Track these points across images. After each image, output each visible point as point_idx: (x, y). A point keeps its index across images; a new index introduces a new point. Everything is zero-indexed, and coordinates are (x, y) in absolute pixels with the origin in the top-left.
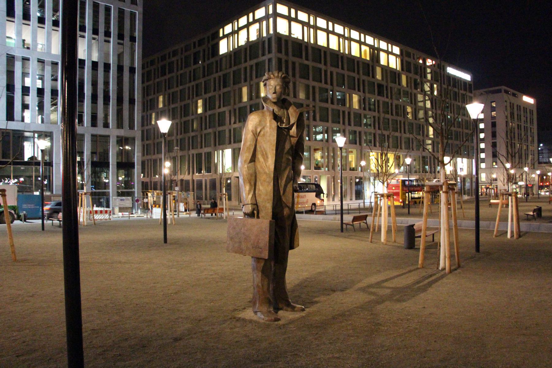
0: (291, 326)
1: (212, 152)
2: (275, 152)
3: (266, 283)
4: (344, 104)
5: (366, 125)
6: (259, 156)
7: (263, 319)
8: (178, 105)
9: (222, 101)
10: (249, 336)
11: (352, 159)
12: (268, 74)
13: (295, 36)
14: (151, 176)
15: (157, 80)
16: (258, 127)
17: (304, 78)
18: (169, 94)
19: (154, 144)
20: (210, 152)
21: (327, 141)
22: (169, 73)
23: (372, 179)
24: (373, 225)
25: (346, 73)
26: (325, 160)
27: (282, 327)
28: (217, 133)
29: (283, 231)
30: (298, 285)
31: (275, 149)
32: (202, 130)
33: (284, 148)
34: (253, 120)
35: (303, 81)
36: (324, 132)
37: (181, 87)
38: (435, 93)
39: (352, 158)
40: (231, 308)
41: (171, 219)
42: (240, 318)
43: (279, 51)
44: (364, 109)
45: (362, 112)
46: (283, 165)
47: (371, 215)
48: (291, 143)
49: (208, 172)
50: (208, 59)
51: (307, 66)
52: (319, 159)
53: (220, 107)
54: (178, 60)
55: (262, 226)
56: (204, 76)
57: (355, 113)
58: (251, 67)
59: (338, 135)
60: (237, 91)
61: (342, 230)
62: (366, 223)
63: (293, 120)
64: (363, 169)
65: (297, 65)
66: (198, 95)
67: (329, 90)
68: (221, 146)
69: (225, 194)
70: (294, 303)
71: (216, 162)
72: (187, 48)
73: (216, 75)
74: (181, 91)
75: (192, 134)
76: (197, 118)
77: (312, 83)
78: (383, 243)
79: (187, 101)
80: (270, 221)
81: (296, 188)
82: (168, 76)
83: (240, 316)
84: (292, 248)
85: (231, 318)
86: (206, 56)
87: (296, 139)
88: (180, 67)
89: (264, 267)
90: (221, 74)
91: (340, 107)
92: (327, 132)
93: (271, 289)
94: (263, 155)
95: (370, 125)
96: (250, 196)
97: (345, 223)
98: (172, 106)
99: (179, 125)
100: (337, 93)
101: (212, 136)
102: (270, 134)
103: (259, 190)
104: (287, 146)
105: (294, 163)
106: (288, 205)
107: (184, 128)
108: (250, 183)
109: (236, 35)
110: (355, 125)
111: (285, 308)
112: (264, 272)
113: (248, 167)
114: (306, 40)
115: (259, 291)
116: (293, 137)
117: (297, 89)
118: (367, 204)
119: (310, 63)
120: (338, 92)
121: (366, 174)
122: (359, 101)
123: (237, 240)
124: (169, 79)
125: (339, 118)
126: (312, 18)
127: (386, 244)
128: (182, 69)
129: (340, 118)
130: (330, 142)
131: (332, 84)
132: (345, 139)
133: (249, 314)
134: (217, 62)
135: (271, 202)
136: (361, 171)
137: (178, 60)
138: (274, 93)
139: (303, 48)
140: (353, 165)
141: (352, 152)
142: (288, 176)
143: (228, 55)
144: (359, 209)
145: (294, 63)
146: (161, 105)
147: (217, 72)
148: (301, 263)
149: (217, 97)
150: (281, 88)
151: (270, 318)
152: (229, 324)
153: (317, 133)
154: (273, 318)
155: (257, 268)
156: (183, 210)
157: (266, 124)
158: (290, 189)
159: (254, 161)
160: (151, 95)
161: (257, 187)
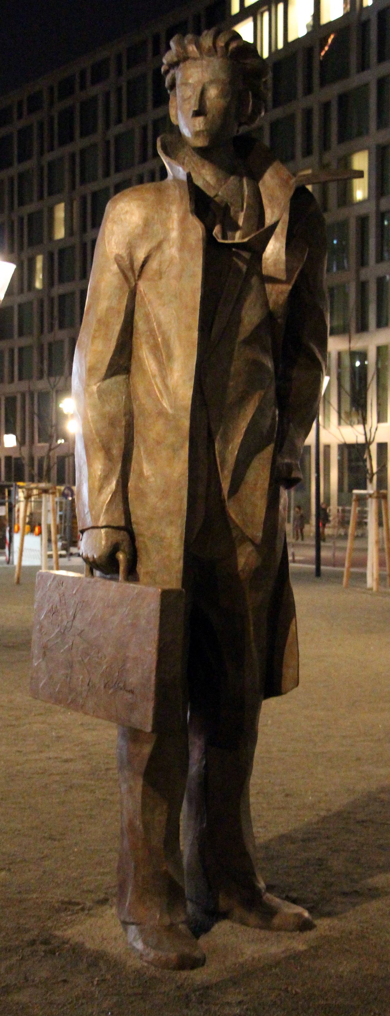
2: (196, 334)
6: (145, 355)
12: (180, 44)
14: (32, 442)
15: (48, 157)
19: (41, 347)
22: (83, 134)
30: (339, 814)
31: (195, 324)
33: (239, 322)
40: (57, 895)
46: (234, 386)
48: (266, 303)
54: (107, 95)
58: (326, 106)
82: (79, 143)
84: (273, 686)
85: (33, 943)
87: (288, 288)
88: (113, 116)
89: (152, 758)
94: (155, 349)
103: (141, 474)
104: (250, 316)
105: (282, 376)
106: (249, 532)
108: (107, 451)
109: (281, 6)
111: (238, 912)
113: (99, 391)
116: (273, 280)
124: (83, 152)
135: (181, 521)
137: (107, 95)
150: (223, 94)
154: (173, 955)
155: (130, 762)
157: (167, 232)
159: (127, 370)
160: (31, 200)
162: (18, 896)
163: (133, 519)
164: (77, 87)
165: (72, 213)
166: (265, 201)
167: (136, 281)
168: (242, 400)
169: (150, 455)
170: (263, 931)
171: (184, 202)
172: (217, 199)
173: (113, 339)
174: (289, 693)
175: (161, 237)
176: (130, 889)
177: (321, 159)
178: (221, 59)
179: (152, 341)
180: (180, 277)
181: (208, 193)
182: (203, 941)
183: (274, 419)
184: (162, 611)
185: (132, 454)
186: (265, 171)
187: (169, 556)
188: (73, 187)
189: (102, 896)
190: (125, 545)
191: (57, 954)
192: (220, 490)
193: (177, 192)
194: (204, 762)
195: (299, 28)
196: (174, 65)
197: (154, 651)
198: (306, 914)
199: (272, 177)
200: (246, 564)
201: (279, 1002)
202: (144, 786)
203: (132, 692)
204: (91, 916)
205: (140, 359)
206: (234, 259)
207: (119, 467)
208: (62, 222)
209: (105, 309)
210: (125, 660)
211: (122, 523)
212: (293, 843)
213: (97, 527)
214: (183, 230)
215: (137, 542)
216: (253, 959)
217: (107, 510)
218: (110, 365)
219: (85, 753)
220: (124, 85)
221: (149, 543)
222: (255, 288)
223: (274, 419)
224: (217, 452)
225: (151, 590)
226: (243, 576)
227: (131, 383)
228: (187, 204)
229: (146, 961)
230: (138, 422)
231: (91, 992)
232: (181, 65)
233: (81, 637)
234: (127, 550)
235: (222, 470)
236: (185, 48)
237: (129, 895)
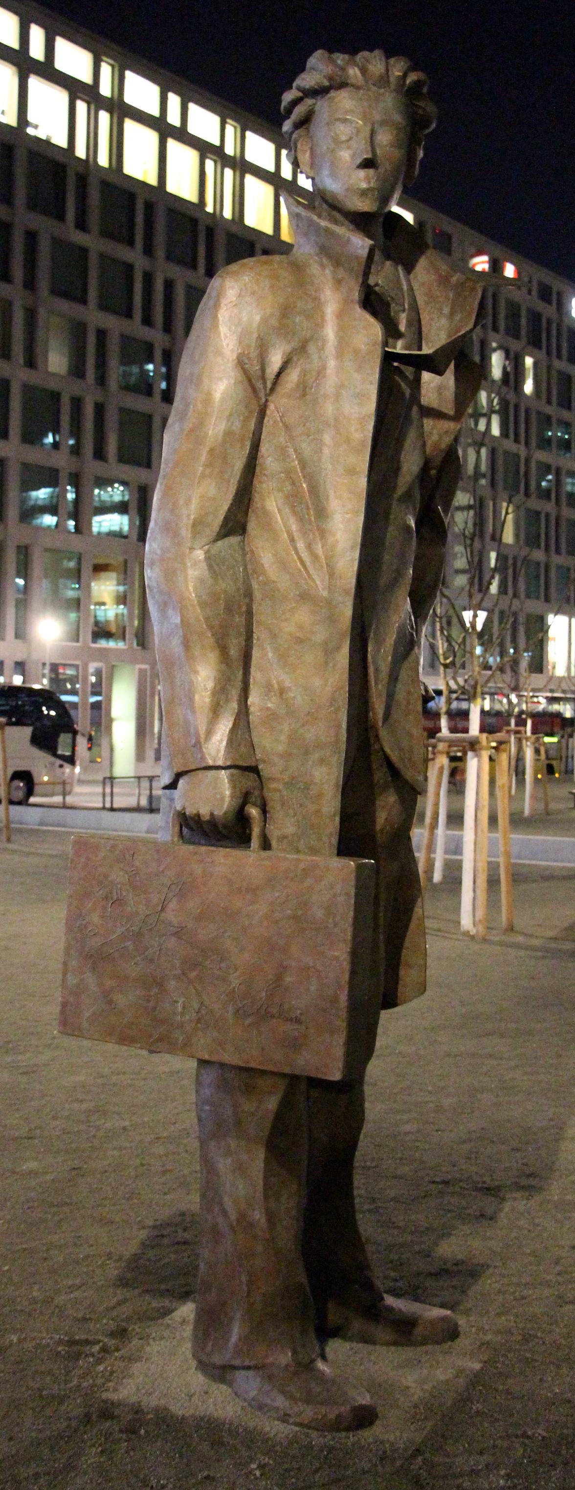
2: (362, 482)
6: (271, 501)
13: (41, 133)
17: (66, 295)
26: (131, 613)
33: (397, 470)
35: (64, 306)
38: (528, 387)
48: (424, 445)
51: (84, 251)
65: (44, 246)
77: (95, 317)
78: (466, 934)
89: (279, 1116)
94: (293, 499)
96: (224, 727)
102: (340, 387)
108: (223, 650)
111: (357, 1325)
113: (209, 558)
114: (81, 152)
116: (437, 414)
117: (40, 334)
119: (91, 241)
126: (106, 70)
127: (484, 940)
157: (320, 325)
172: (377, 289)
173: (232, 481)
178: (394, 94)
179: (289, 488)
193: (327, 271)
197: (345, 956)
203: (298, 1021)
206: (397, 378)
207: (240, 674)
209: (221, 433)
210: (282, 971)
222: (415, 423)
230: (262, 612)
232: (333, 94)
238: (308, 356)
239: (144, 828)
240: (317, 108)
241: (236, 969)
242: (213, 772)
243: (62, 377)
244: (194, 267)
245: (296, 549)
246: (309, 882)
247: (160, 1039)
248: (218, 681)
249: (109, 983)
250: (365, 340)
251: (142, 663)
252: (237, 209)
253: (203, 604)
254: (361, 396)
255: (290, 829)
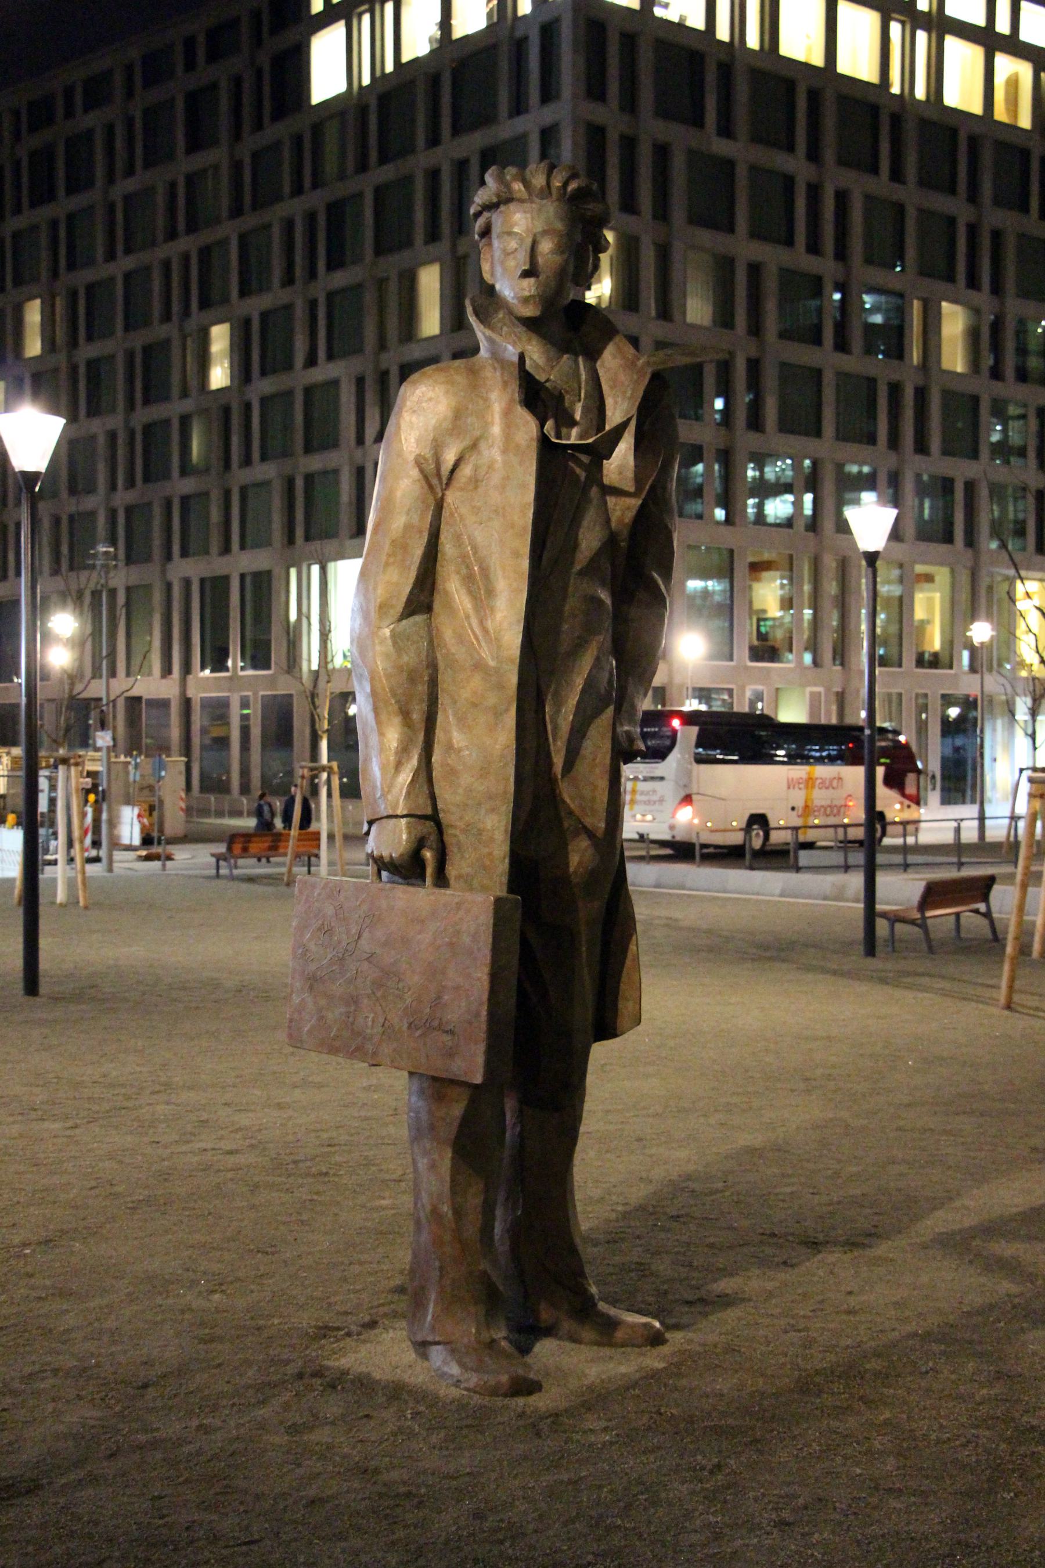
0: (592, 1422)
1: (277, 571)
2: (525, 564)
3: (474, 1200)
4: (898, 352)
5: (1002, 449)
6: (452, 585)
7: (457, 1383)
8: (113, 346)
9: (322, 334)
10: (376, 1471)
11: (930, 609)
12: (500, 179)
16: (453, 438)
18: (73, 295)
20: (269, 573)
21: (813, 525)
22: (70, 191)
23: (1022, 707)
24: (1020, 923)
25: (911, 195)
27: (544, 1426)
28: (299, 483)
29: (564, 947)
30: (641, 1208)
31: (526, 550)
32: (227, 465)
33: (576, 546)
34: (422, 411)
35: (705, 237)
36: (800, 484)
37: (127, 263)
39: (929, 606)
40: (306, 1320)
41: (71, 884)
42: (345, 1373)
43: (595, 91)
44: (996, 374)
45: (987, 390)
47: (1010, 878)
48: (608, 521)
49: (255, 667)
50: (258, 126)
51: (728, 165)
52: (774, 611)
53: (311, 361)
54: (110, 129)
55: (457, 924)
56: (237, 211)
57: (948, 395)
59: (868, 497)
60: (393, 287)
61: (870, 947)
62: (988, 915)
63: (618, 409)
64: (981, 660)
65: (678, 163)
66: (210, 302)
67: (828, 285)
68: (316, 545)
69: (330, 771)
70: (614, 1302)
71: (293, 616)
72: (155, 69)
73: (294, 207)
74: (128, 276)
75: (187, 486)
76: (204, 412)
77: (746, 249)
79: (160, 331)
80: (498, 901)
81: (631, 740)
82: (64, 205)
83: (344, 1362)
84: (606, 1028)
85: (300, 1376)
86: (247, 111)
87: (636, 503)
89: (466, 1121)
90: (316, 200)
91: (878, 366)
92: (812, 483)
93: (498, 1228)
94: (469, 580)
95: (1022, 452)
96: (405, 777)
97: (884, 915)
98: (87, 351)
99: (121, 440)
100: (868, 301)
101: (277, 503)
103: (449, 747)
104: (589, 540)
105: (619, 618)
106: (588, 821)
107: (146, 452)
108: (405, 714)
110: (946, 452)
111: (567, 1325)
112: (471, 1146)
113: (394, 635)
115: (438, 1242)
117: (676, 275)
118: (997, 830)
120: (870, 290)
121: (993, 684)
122: (973, 335)
123: (337, 988)
124: (70, 217)
125: (872, 415)
128: (130, 172)
129: (872, 415)
130: (825, 526)
131: (841, 254)
132: (892, 513)
133: (387, 1354)
134: (298, 140)
135: (506, 808)
136: (973, 669)
137: (110, 129)
138: (526, 274)
139: (711, 76)
140: (935, 642)
141: (929, 578)
142: (590, 684)
143: (349, 107)
144: (958, 849)
145: (662, 152)
146: (34, 347)
147: (298, 190)
148: (640, 1113)
149: (300, 312)
150: (559, 249)
151: (492, 1380)
152: (286, 1407)
153: (765, 490)
154: (504, 1378)
155: (432, 1128)
156: (137, 841)
157: (486, 425)
158: (597, 745)
159: (428, 609)
161: (439, 734)
162: (253, 1323)
163: (440, 806)
164: (60, 112)
165: (53, 313)
166: (605, 387)
167: (443, 490)
168: (579, 646)
169: (461, 720)
170: (601, 1349)
171: (509, 390)
172: (548, 384)
174: (625, 1036)
175: (478, 433)
176: (433, 1297)
177: (454, 246)
178: (557, 203)
180: (502, 488)
181: (537, 377)
182: (529, 1359)
183: (611, 674)
184: (495, 925)
185: (436, 719)
186: (604, 348)
187: (490, 854)
188: (55, 274)
189: (367, 1319)
190: (433, 838)
191: (339, 1387)
192: (550, 764)
193: (498, 374)
194: (518, 1129)
195: (418, 41)
196: (490, 207)
198: (657, 1324)
199: (614, 357)
200: (580, 863)
201: (654, 1426)
202: (453, 1158)
203: (451, 1032)
204: (365, 1341)
205: (446, 593)
207: (421, 737)
208: (37, 329)
209: (402, 525)
211: (429, 811)
212: (595, 1246)
213: (397, 816)
214: (508, 426)
215: (445, 836)
216: (602, 1381)
217: (408, 793)
218: (409, 601)
219: (254, 1142)
220: (138, 115)
221: (462, 837)
222: (595, 502)
223: (611, 674)
224: (547, 717)
225: (479, 898)
226: (575, 880)
227: (433, 625)
228: (514, 390)
229: (466, 1389)
230: (445, 679)
231: (409, 1427)
232: (502, 208)
233: (370, 962)
234: (434, 846)
235: (554, 740)
236: (508, 186)
237: (432, 1305)
238: (479, 453)
239: (778, 891)
240: (493, 220)
241: (409, 989)
242: (394, 820)
243: (706, 328)
244: (874, 170)
245: (470, 624)
246: (461, 913)
247: (357, 1049)
248: (401, 741)
249: (323, 1002)
250: (526, 437)
251: (815, 685)
252: (933, 85)
253: (388, 676)
254: (523, 486)
255: (466, 870)
